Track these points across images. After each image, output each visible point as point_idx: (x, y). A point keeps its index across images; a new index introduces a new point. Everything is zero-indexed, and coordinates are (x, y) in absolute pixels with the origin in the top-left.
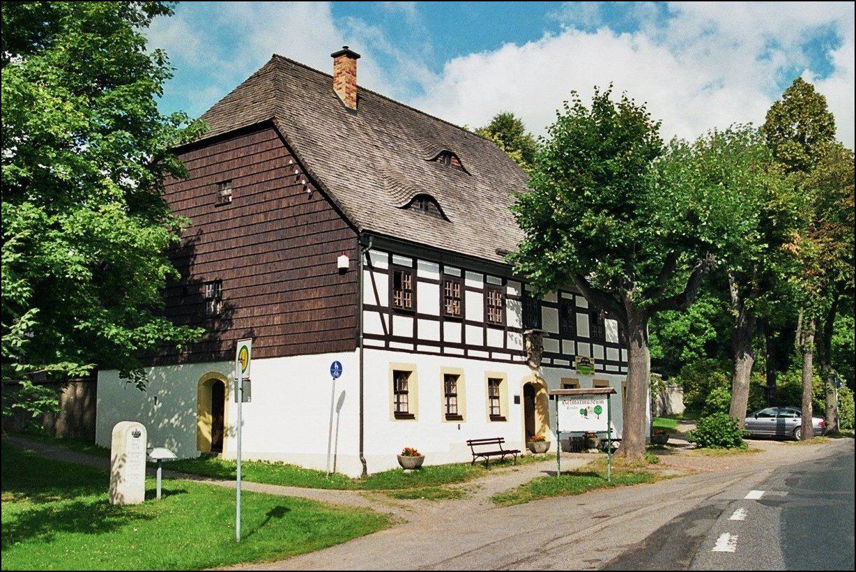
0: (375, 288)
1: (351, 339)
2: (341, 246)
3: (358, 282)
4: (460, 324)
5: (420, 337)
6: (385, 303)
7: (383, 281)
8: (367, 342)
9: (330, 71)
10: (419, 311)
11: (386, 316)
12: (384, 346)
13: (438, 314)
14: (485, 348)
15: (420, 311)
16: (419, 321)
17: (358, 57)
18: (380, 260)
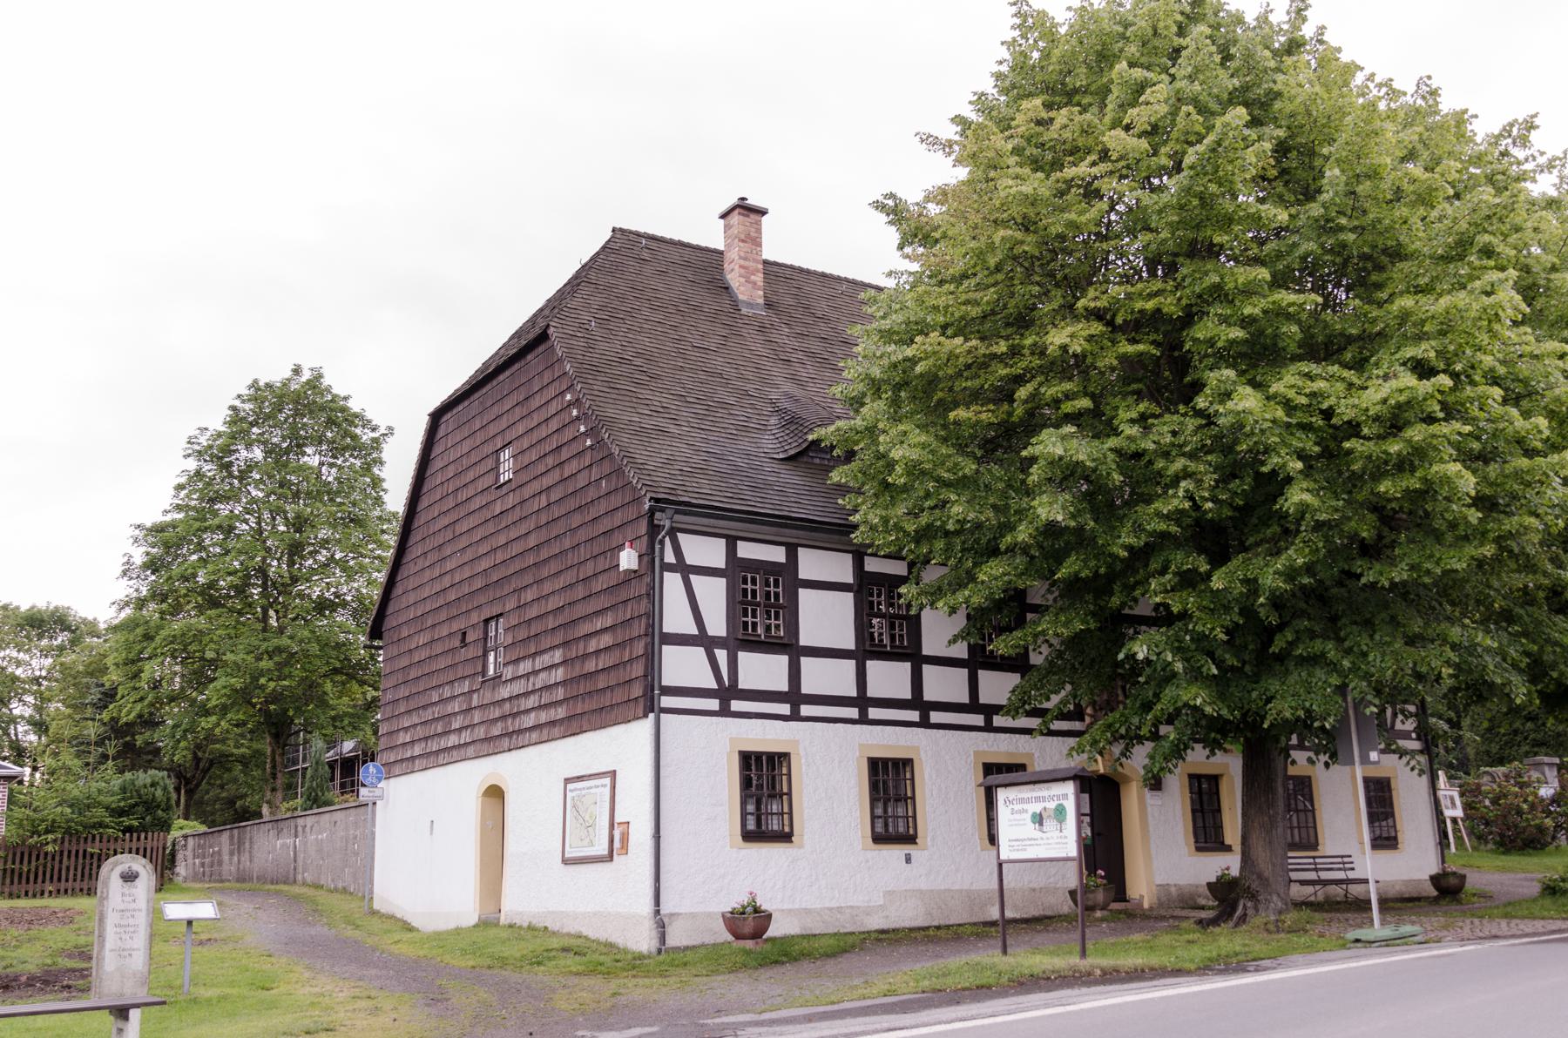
0: (694, 600)
1: (648, 697)
2: (616, 539)
3: (653, 596)
4: (908, 665)
5: (805, 690)
6: (717, 626)
7: (713, 595)
8: (667, 702)
9: (718, 243)
10: (803, 642)
11: (721, 655)
12: (788, 713)
13: (852, 646)
14: (974, 706)
15: (804, 641)
16: (926, 668)
17: (763, 212)
18: (705, 550)
